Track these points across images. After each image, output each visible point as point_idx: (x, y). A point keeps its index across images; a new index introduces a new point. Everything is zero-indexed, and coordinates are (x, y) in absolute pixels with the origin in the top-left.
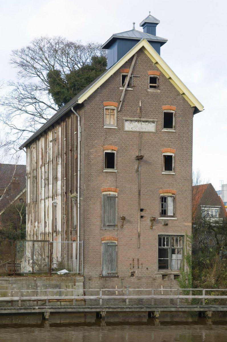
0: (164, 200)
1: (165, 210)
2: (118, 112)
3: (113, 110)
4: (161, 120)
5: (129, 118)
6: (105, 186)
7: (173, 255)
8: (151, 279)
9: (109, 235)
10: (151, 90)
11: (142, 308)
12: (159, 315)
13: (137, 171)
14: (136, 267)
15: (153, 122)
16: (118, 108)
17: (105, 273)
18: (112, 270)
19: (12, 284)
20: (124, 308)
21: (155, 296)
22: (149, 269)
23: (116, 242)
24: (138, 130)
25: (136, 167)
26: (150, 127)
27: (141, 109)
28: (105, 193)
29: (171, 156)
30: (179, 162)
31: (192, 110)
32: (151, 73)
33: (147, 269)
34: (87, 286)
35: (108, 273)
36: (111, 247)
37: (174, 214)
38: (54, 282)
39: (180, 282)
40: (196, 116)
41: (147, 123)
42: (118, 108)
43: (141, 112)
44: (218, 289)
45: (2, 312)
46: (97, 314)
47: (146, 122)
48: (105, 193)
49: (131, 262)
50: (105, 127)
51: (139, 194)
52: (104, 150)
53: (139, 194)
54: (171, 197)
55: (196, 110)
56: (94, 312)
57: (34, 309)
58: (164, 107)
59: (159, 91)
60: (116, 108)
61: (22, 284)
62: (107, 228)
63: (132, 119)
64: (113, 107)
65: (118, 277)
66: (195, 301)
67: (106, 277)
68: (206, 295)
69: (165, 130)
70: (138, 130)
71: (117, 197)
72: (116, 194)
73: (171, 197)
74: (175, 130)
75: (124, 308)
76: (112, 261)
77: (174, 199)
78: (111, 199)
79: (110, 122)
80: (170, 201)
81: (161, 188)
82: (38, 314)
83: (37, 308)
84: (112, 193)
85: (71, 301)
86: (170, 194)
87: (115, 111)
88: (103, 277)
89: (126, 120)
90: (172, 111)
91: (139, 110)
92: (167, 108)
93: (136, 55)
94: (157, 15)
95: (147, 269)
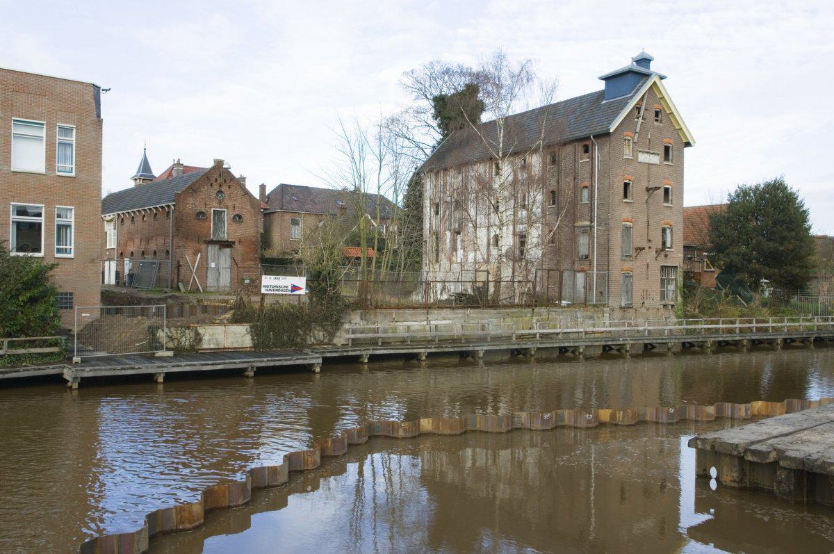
0: (664, 230)
3: (629, 140)
4: (662, 151)
5: (641, 150)
6: (625, 216)
7: (587, 254)
9: (627, 265)
10: (656, 123)
11: (698, 338)
13: (647, 202)
15: (658, 154)
17: (623, 305)
21: (687, 327)
25: (646, 198)
26: (655, 159)
27: (650, 141)
28: (623, 223)
32: (656, 107)
34: (612, 318)
36: (628, 277)
39: (675, 312)
40: (686, 150)
43: (649, 143)
44: (596, 299)
47: (653, 154)
48: (623, 223)
51: (648, 225)
53: (648, 225)
55: (688, 144)
62: (625, 258)
64: (629, 138)
67: (624, 308)
68: (686, 325)
69: (665, 163)
78: (627, 229)
80: (668, 231)
81: (663, 220)
82: (481, 349)
83: (621, 339)
84: (628, 223)
86: (669, 226)
88: (621, 308)
90: (670, 145)
93: (647, 94)
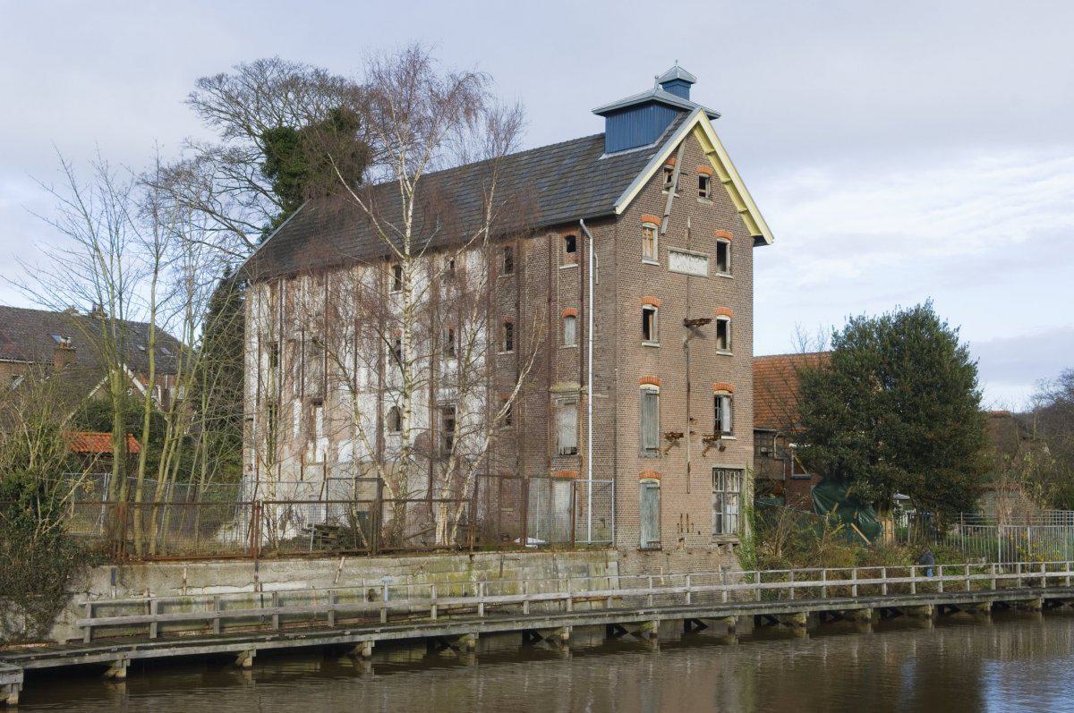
0: (718, 401)
1: (719, 422)
2: (661, 235)
3: (652, 230)
8: (705, 553)
10: (700, 200)
12: (805, 620)
13: (686, 346)
14: (685, 531)
15: (705, 258)
16: (660, 229)
17: (644, 544)
18: (653, 536)
19: (523, 566)
20: (761, 608)
22: (702, 534)
23: (658, 481)
24: (685, 270)
27: (689, 233)
28: (643, 386)
29: (726, 321)
30: (737, 334)
31: (752, 241)
32: (701, 170)
33: (699, 533)
35: (648, 543)
37: (732, 430)
38: (580, 562)
40: (758, 251)
41: (697, 259)
42: (660, 229)
45: (453, 633)
46: (685, 624)
48: (643, 386)
49: (678, 521)
50: (644, 261)
51: (689, 391)
52: (642, 305)
53: (689, 391)
54: (727, 397)
56: (600, 625)
57: (637, 614)
58: (720, 232)
59: (711, 203)
60: (656, 228)
61: (537, 567)
63: (679, 249)
65: (660, 549)
66: (769, 596)
70: (686, 271)
71: (659, 395)
72: (657, 388)
73: (727, 397)
74: (731, 274)
75: (761, 608)
76: (656, 519)
77: (731, 400)
78: (650, 396)
79: (650, 253)
80: (725, 402)
83: (641, 612)
84: (652, 387)
85: (604, 599)
87: (655, 234)
89: (672, 252)
91: (687, 235)
92: (720, 235)
94: (689, 68)
95: (699, 533)
